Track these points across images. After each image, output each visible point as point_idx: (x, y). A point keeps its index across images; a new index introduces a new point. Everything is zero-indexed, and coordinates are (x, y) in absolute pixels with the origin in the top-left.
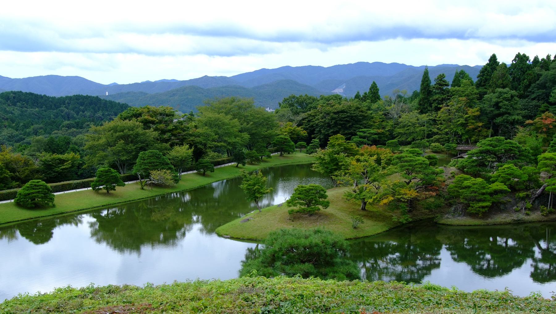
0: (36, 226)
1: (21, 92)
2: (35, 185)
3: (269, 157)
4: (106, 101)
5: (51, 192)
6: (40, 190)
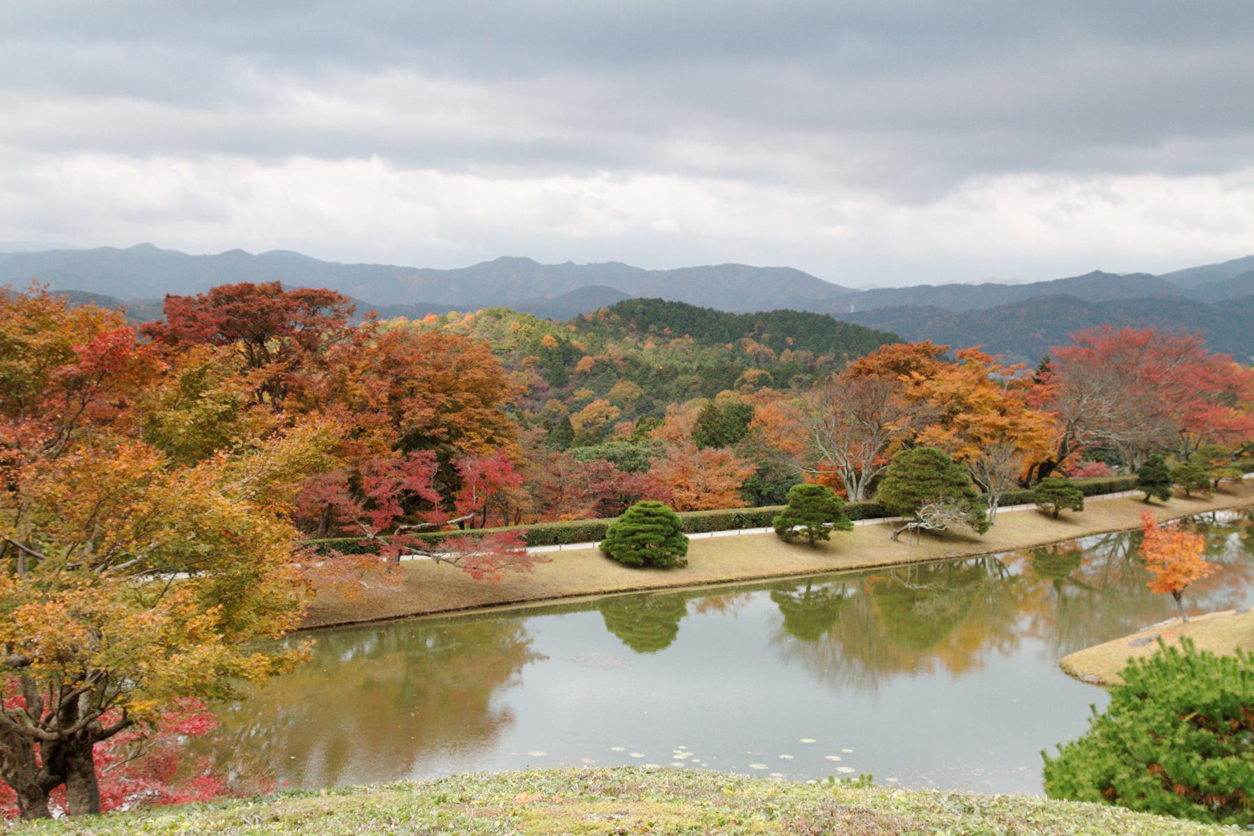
1: (661, 301)
2: (647, 514)
4: (847, 326)
5: (683, 530)
6: (659, 526)
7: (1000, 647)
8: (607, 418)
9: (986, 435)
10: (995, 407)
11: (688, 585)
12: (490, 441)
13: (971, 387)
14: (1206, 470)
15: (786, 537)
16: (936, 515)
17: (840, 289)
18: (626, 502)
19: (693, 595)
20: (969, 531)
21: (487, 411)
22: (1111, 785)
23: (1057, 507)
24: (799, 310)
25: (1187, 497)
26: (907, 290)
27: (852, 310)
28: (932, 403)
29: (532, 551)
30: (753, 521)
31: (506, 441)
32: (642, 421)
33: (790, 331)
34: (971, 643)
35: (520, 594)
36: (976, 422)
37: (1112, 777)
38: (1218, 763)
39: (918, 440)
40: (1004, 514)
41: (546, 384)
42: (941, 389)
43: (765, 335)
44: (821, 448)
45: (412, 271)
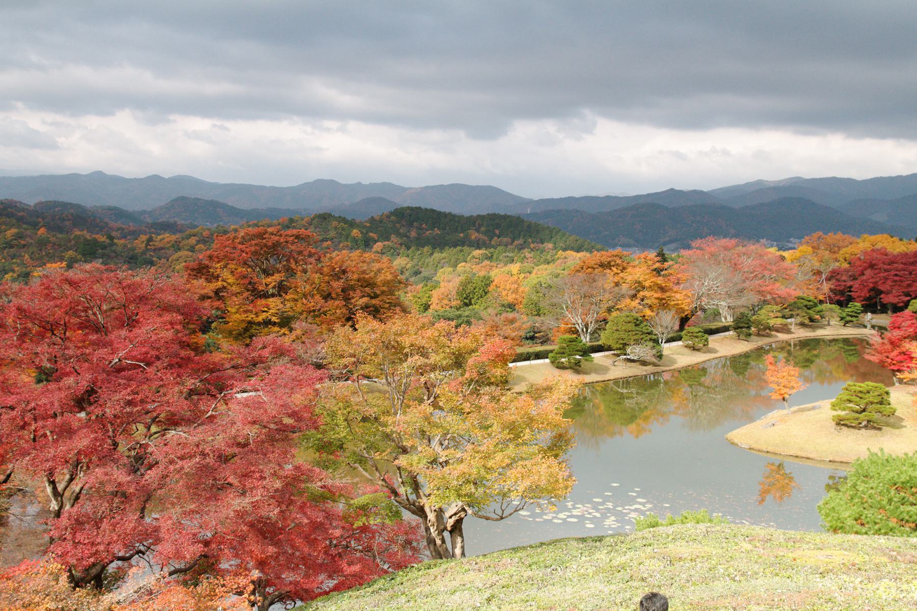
13: (647, 277)
24: (502, 213)
26: (561, 200)
33: (498, 226)
45: (262, 188)
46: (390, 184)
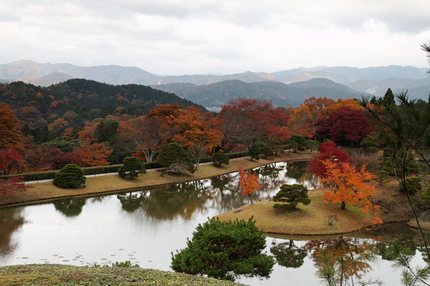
0: (68, 203)
1: (84, 80)
2: (70, 169)
3: (282, 152)
6: (75, 173)
7: (202, 212)
8: (63, 125)
9: (196, 138)
10: (199, 128)
11: (85, 194)
12: (11, 142)
14: (272, 149)
15: (122, 176)
16: (177, 167)
17: (155, 76)
18: (65, 163)
19: (89, 197)
20: (188, 172)
21: (9, 131)
22: (189, 262)
23: (220, 163)
25: (265, 158)
27: (159, 84)
28: (177, 126)
29: (26, 183)
30: (111, 170)
31: (17, 142)
32: (75, 128)
34: (190, 212)
35: (22, 199)
36: (192, 133)
37: (189, 260)
38: (218, 254)
39: (172, 140)
40: (201, 166)
41: (38, 112)
42: (180, 121)
43: (125, 94)
44: (137, 143)
46: (69, 64)
